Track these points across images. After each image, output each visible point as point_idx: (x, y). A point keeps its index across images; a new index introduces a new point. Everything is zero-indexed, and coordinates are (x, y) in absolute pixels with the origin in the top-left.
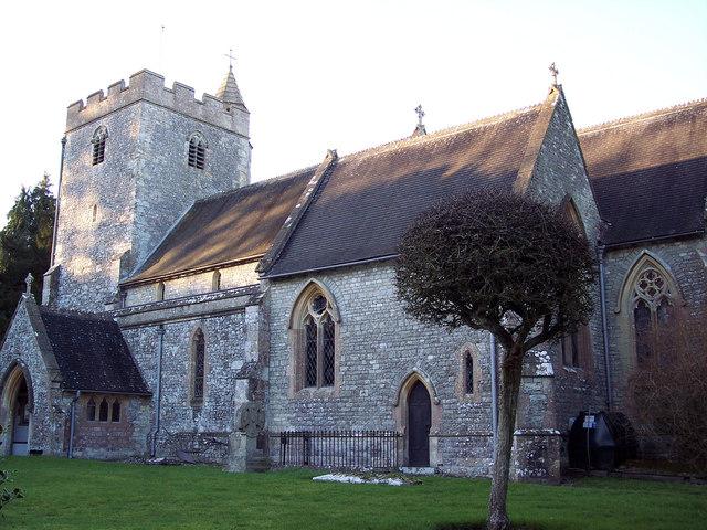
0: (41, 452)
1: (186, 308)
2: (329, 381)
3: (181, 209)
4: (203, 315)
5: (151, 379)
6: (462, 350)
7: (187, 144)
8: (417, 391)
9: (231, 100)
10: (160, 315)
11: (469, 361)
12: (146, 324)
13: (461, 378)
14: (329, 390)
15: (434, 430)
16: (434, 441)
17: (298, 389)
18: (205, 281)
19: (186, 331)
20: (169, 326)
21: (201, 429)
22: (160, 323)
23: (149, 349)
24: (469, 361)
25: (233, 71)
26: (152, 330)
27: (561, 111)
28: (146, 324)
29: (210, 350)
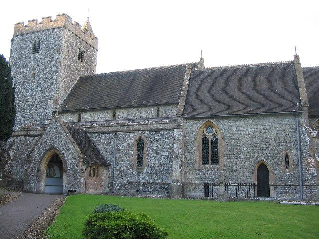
0: (75, 191)
1: (131, 127)
2: (215, 161)
3: (75, 79)
4: (142, 131)
5: (108, 158)
6: (284, 153)
7: (78, 50)
8: (262, 170)
9: (88, 30)
10: (115, 129)
11: (287, 157)
12: (105, 133)
13: (284, 163)
14: (216, 166)
15: (271, 183)
16: (271, 188)
17: (200, 165)
18: (106, 116)
19: (132, 139)
20: (120, 135)
21: (143, 181)
22: (115, 133)
23: (106, 144)
24: (287, 157)
25: (89, 20)
26: (112, 135)
27: (202, 62)
28: (105, 133)
29: (147, 148)
